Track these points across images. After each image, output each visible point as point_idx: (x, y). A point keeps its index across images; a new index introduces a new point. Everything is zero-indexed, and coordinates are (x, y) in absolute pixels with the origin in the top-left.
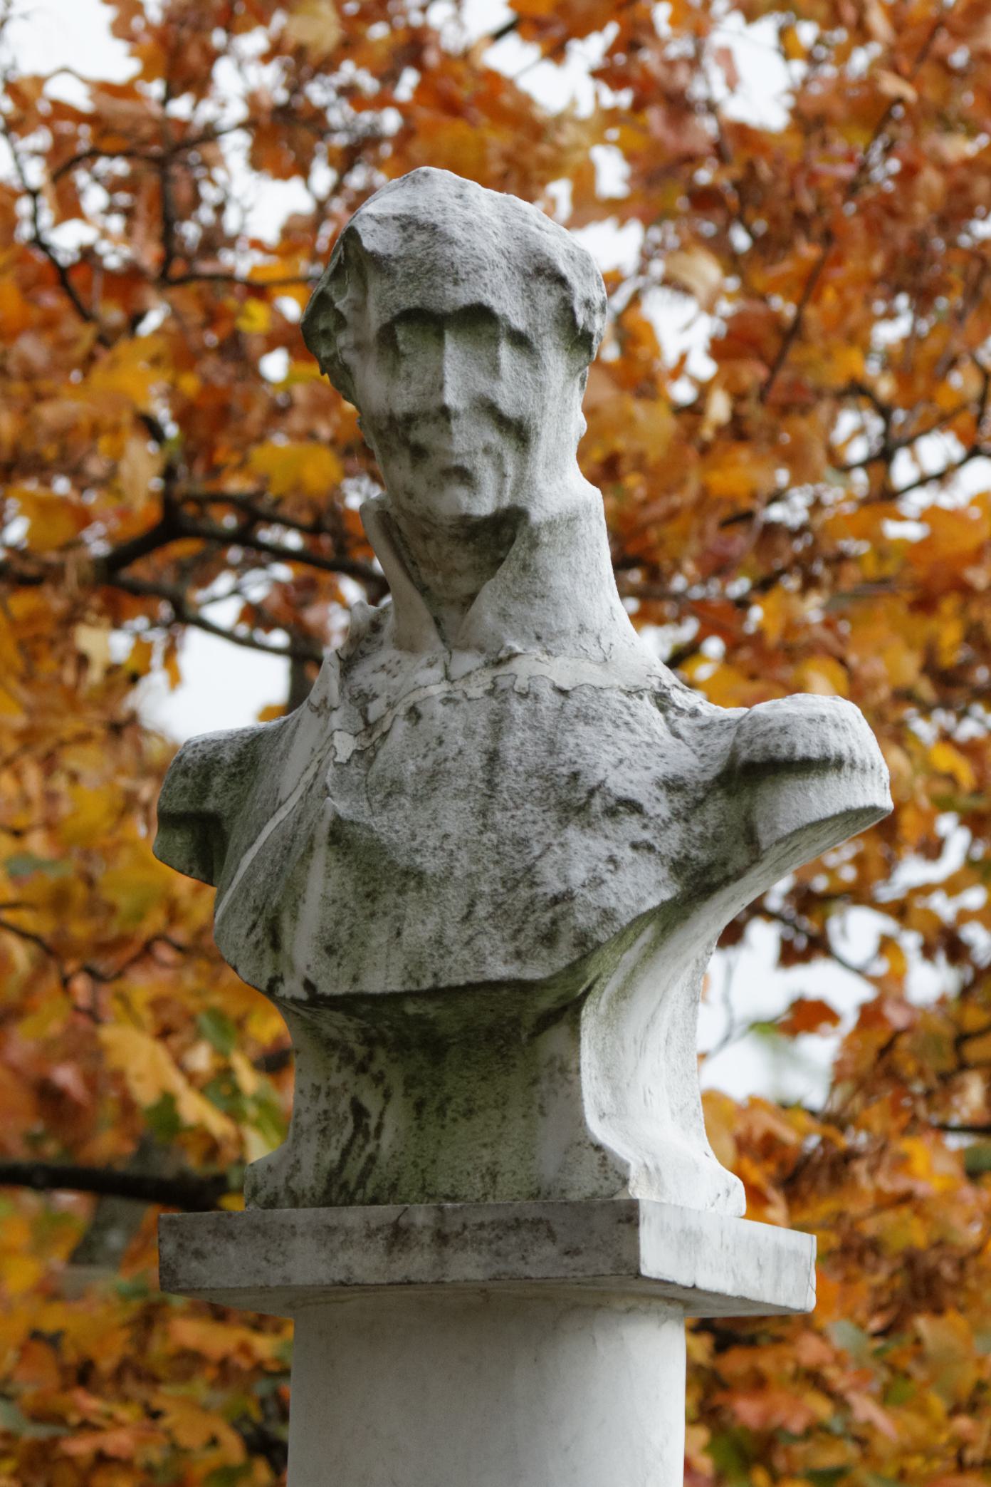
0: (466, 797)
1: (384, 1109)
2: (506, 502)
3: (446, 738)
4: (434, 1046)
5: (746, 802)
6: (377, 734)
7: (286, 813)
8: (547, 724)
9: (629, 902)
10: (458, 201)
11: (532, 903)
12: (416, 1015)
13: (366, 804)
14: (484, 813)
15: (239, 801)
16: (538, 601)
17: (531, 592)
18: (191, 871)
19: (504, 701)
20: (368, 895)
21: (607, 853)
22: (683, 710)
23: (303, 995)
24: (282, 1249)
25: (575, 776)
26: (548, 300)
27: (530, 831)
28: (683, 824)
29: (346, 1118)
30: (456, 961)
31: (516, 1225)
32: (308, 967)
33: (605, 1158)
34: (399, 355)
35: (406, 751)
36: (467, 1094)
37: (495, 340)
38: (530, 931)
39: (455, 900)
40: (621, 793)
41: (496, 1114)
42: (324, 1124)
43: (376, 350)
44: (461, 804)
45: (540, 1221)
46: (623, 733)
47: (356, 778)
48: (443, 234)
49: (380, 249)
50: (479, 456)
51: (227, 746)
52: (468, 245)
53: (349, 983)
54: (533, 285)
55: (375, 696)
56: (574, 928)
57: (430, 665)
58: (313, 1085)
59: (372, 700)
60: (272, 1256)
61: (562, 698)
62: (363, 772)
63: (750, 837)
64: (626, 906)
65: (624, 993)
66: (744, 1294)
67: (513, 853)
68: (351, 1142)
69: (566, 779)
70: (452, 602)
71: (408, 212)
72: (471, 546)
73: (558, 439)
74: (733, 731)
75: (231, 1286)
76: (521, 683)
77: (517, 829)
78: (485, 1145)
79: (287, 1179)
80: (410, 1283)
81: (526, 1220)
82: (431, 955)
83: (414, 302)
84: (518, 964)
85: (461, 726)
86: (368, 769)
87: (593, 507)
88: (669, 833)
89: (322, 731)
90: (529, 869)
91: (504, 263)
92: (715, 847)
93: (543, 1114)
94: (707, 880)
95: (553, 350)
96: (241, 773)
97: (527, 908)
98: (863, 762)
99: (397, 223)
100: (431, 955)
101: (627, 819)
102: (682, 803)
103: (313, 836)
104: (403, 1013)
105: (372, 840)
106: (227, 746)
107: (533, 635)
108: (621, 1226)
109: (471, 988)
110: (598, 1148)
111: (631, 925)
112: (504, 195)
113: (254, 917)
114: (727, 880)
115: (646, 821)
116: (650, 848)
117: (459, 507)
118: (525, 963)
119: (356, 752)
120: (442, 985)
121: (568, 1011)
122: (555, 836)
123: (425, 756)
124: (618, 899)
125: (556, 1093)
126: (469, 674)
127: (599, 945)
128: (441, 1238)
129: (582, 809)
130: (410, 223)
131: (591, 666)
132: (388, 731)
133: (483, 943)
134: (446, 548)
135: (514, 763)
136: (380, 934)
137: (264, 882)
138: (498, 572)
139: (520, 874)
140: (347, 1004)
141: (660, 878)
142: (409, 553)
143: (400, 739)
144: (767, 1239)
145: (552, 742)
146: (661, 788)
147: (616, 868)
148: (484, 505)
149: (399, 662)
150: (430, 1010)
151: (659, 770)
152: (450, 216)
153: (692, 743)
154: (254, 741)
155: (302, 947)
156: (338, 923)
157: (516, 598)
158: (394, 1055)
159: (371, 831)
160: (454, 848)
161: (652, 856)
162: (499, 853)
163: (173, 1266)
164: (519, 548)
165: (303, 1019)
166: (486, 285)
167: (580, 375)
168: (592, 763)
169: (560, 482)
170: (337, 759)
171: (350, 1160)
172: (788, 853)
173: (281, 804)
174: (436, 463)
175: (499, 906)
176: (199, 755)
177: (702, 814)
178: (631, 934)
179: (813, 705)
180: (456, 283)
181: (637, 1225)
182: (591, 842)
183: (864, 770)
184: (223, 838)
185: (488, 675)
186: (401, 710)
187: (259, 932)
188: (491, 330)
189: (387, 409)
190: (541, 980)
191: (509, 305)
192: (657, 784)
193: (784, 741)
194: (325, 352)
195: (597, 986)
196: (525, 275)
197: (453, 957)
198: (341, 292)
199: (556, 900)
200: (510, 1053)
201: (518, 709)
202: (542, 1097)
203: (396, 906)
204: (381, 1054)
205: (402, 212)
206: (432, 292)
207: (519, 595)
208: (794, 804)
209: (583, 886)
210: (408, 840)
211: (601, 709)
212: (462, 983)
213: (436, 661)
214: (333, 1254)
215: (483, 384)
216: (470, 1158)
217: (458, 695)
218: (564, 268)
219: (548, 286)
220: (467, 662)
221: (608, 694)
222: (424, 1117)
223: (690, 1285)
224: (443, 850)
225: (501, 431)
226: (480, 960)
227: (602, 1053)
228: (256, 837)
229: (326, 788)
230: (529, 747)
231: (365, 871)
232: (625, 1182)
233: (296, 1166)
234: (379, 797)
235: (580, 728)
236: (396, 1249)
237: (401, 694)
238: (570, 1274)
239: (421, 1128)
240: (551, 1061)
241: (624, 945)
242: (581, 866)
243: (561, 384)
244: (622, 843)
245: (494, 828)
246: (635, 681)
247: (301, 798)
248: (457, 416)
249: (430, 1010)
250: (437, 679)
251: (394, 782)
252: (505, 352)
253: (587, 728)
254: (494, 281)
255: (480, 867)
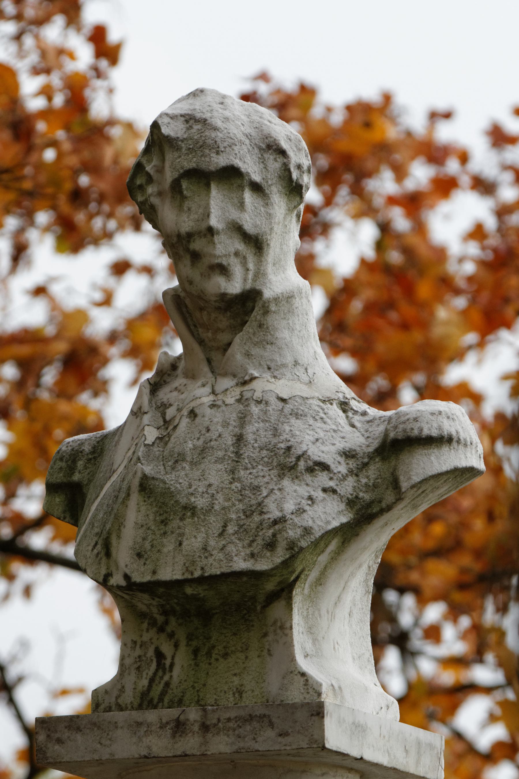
0: (222, 462)
1: (175, 654)
2: (248, 286)
3: (212, 428)
4: (205, 615)
5: (393, 463)
6: (171, 427)
7: (116, 476)
8: (273, 419)
9: (320, 523)
10: (221, 106)
11: (261, 524)
12: (192, 594)
13: (162, 468)
14: (233, 472)
15: (92, 475)
16: (269, 346)
17: (264, 340)
18: (65, 518)
19: (247, 406)
20: (162, 522)
21: (307, 494)
22: (357, 412)
23: (123, 583)
24: (109, 737)
25: (289, 449)
26: (274, 165)
27: (261, 481)
28: (355, 478)
29: (152, 660)
30: (215, 560)
31: (251, 718)
32: (126, 566)
33: (307, 680)
34: (184, 198)
35: (188, 436)
36: (225, 644)
37: (241, 188)
38: (259, 541)
39: (215, 523)
40: (317, 458)
41: (242, 656)
42: (139, 664)
43: (170, 195)
44: (220, 466)
45: (265, 715)
46: (319, 424)
47: (157, 453)
48: (210, 125)
49: (172, 134)
50: (232, 257)
51: (87, 443)
52: (225, 131)
53: (150, 574)
54: (266, 156)
55: (171, 405)
56: (286, 539)
57: (204, 386)
58: (132, 640)
59: (168, 408)
60: (103, 741)
61: (283, 404)
62: (161, 449)
63: (395, 484)
64: (318, 525)
65: (320, 582)
66: (395, 766)
67: (250, 495)
68: (155, 674)
69: (283, 450)
70: (218, 349)
71: (190, 112)
72: (229, 314)
73: (282, 249)
74: (386, 423)
75: (79, 760)
76: (258, 395)
77: (253, 480)
78: (235, 675)
79: (117, 698)
80: (186, 755)
81: (256, 716)
82: (200, 557)
83: (192, 165)
84: (252, 561)
85: (221, 421)
86: (164, 448)
87: (303, 291)
88: (346, 483)
89: (138, 426)
90: (259, 504)
91: (247, 142)
92: (374, 491)
93: (270, 655)
94: (369, 511)
95: (278, 195)
96: (95, 458)
97: (258, 527)
98: (465, 440)
99: (183, 119)
100: (200, 557)
101: (320, 474)
102: (355, 465)
103: (130, 487)
104: (185, 594)
105: (165, 488)
106: (87, 443)
107: (266, 367)
108: (313, 718)
109: (224, 576)
110: (303, 674)
111: (322, 537)
112: (249, 103)
113: (96, 539)
114: (382, 511)
115: (332, 475)
116: (334, 491)
117: (219, 288)
118: (256, 560)
119: (158, 438)
120: (206, 574)
121: (284, 592)
122: (276, 485)
123: (199, 439)
124: (314, 521)
125: (278, 642)
126: (227, 390)
127: (301, 549)
128: (205, 728)
129: (293, 468)
130: (191, 119)
131: (301, 385)
132: (177, 425)
133: (231, 548)
134: (213, 315)
135: (252, 442)
136: (169, 545)
137: (102, 517)
138: (244, 328)
139: (255, 507)
140: (150, 588)
141: (340, 510)
142: (192, 320)
143: (184, 429)
144: (411, 735)
145: (276, 429)
146: (341, 456)
147: (313, 503)
148: (235, 286)
149: (185, 385)
150: (200, 591)
151: (341, 445)
152: (215, 114)
153: (362, 430)
154: (102, 439)
155: (123, 554)
156: (144, 539)
157: (256, 344)
158: (180, 621)
159: (165, 483)
160: (215, 492)
161: (335, 497)
162: (241, 495)
163: (44, 749)
164: (256, 314)
165: (126, 600)
166: (236, 154)
167: (295, 212)
168: (299, 441)
169: (283, 275)
170: (146, 442)
171: (154, 686)
172: (420, 495)
173: (114, 472)
174: (206, 261)
175: (241, 526)
176: (70, 448)
177: (367, 471)
178: (322, 544)
179: (435, 405)
180: (218, 153)
181: (323, 717)
182: (298, 488)
183: (466, 445)
184: (83, 497)
185: (238, 391)
186: (185, 412)
187: (99, 547)
188: (239, 182)
189: (176, 230)
190: (266, 571)
191: (251, 167)
192: (339, 453)
193: (416, 426)
194: (140, 199)
195: (303, 576)
196: (260, 149)
197: (213, 558)
198: (149, 161)
199: (275, 522)
200: (250, 618)
201: (255, 409)
202: (269, 645)
203: (179, 528)
204: (173, 621)
205: (186, 112)
206: (203, 159)
207: (257, 342)
208: (422, 464)
209: (292, 513)
210: (187, 488)
211: (306, 410)
212: (218, 573)
213: (207, 383)
214: (140, 739)
215: (234, 214)
216: (226, 683)
217: (219, 403)
218: (285, 145)
219: (275, 156)
220: (226, 383)
221: (311, 401)
222: (199, 658)
223: (359, 757)
224: (208, 493)
225: (245, 243)
226: (229, 559)
227: (306, 618)
228: (100, 493)
229: (139, 459)
230: (262, 433)
231: (160, 507)
232: (319, 694)
233: (122, 690)
234: (170, 463)
235: (293, 420)
236: (177, 735)
237: (185, 403)
238: (283, 748)
239: (197, 665)
240: (275, 622)
241: (318, 551)
242: (291, 502)
243: (283, 216)
244: (317, 488)
245: (239, 480)
246: (328, 394)
247: (125, 467)
248: (218, 233)
249: (200, 591)
250: (207, 393)
251: (179, 454)
252: (248, 196)
253: (297, 421)
254: (241, 152)
255: (230, 503)
